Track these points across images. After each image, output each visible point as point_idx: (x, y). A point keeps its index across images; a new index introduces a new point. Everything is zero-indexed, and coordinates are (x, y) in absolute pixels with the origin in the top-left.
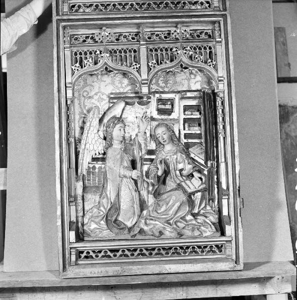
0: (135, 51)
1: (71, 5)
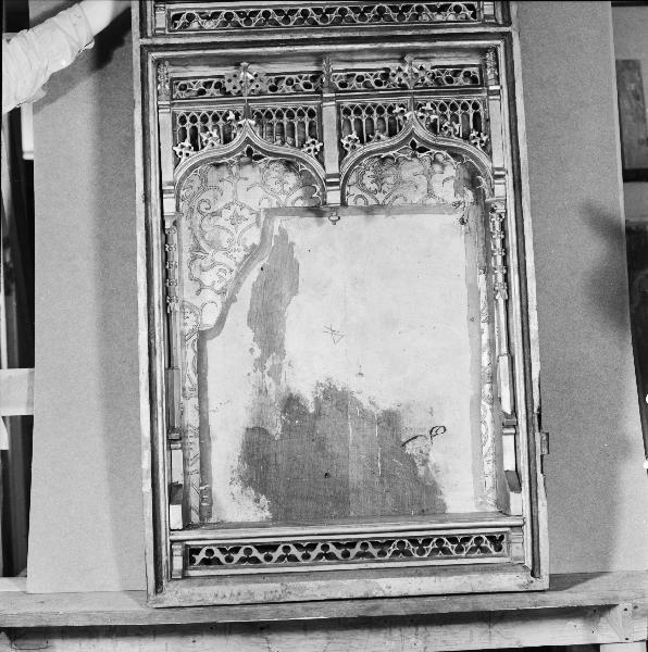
0: (311, 114)
1: (172, 14)
